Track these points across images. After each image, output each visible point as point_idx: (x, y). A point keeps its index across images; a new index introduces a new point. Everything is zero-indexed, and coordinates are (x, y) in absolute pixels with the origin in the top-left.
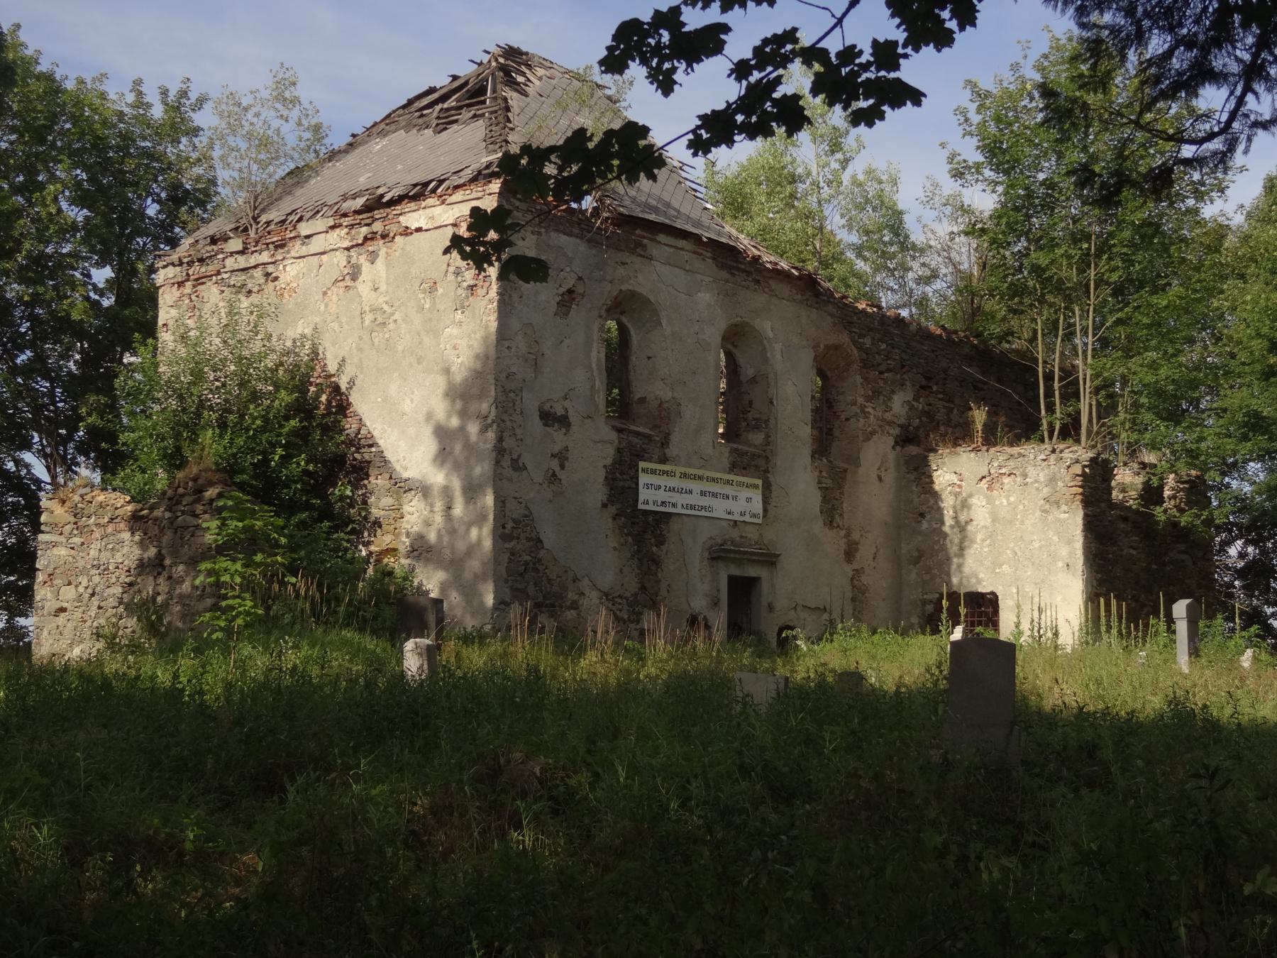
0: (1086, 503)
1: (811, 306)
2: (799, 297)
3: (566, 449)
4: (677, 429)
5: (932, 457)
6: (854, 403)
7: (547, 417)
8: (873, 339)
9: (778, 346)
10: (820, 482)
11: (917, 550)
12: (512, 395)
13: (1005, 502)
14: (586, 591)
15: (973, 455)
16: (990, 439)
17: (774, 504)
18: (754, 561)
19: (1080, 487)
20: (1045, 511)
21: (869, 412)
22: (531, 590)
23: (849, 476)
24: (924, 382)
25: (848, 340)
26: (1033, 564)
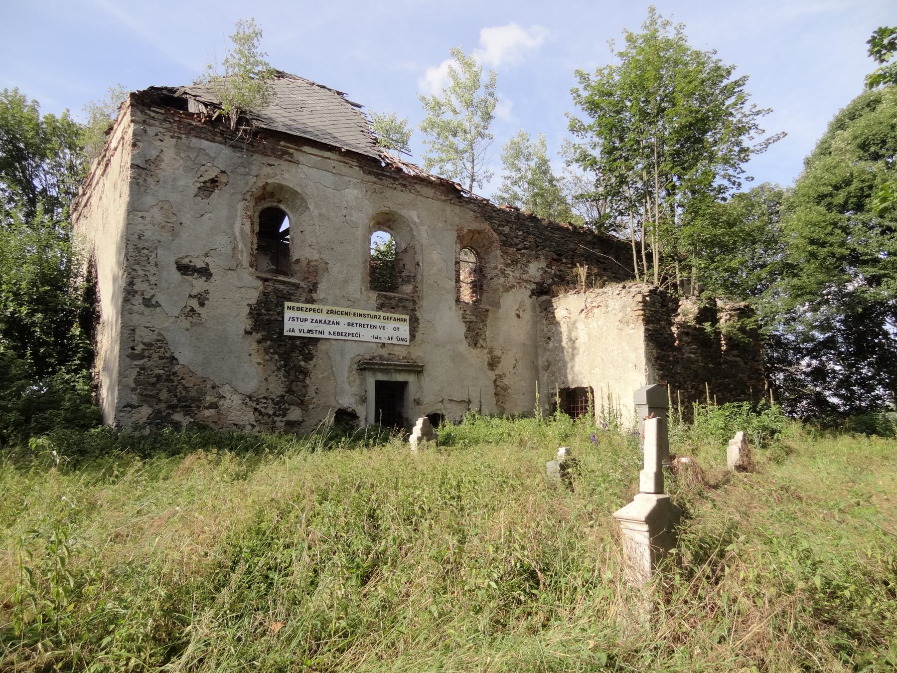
0: (647, 321)
1: (454, 204)
2: (443, 197)
4: (324, 280)
5: (554, 300)
6: (496, 268)
7: (184, 269)
8: (511, 228)
9: (424, 229)
10: (464, 318)
11: (547, 361)
12: (146, 252)
13: (595, 325)
15: (576, 296)
16: (590, 285)
17: (421, 332)
19: (642, 310)
20: (621, 329)
21: (509, 274)
23: (490, 314)
24: (555, 257)
25: (488, 227)
26: (614, 366)
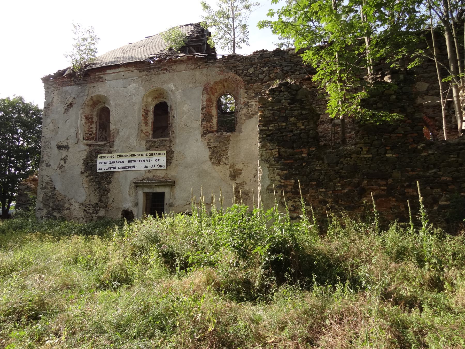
3: (67, 156)
7: (60, 147)
12: (47, 143)
14: (73, 204)
18: (162, 186)
22: (51, 204)
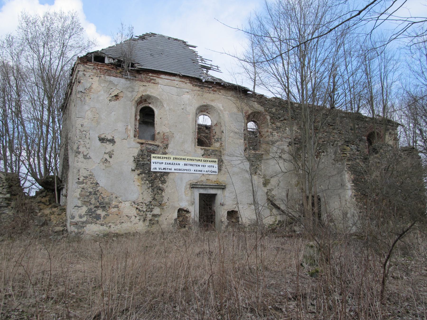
3: (113, 151)
4: (172, 142)
12: (84, 132)
21: (275, 134)
